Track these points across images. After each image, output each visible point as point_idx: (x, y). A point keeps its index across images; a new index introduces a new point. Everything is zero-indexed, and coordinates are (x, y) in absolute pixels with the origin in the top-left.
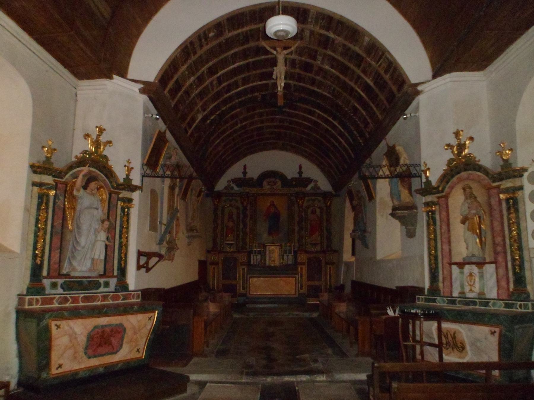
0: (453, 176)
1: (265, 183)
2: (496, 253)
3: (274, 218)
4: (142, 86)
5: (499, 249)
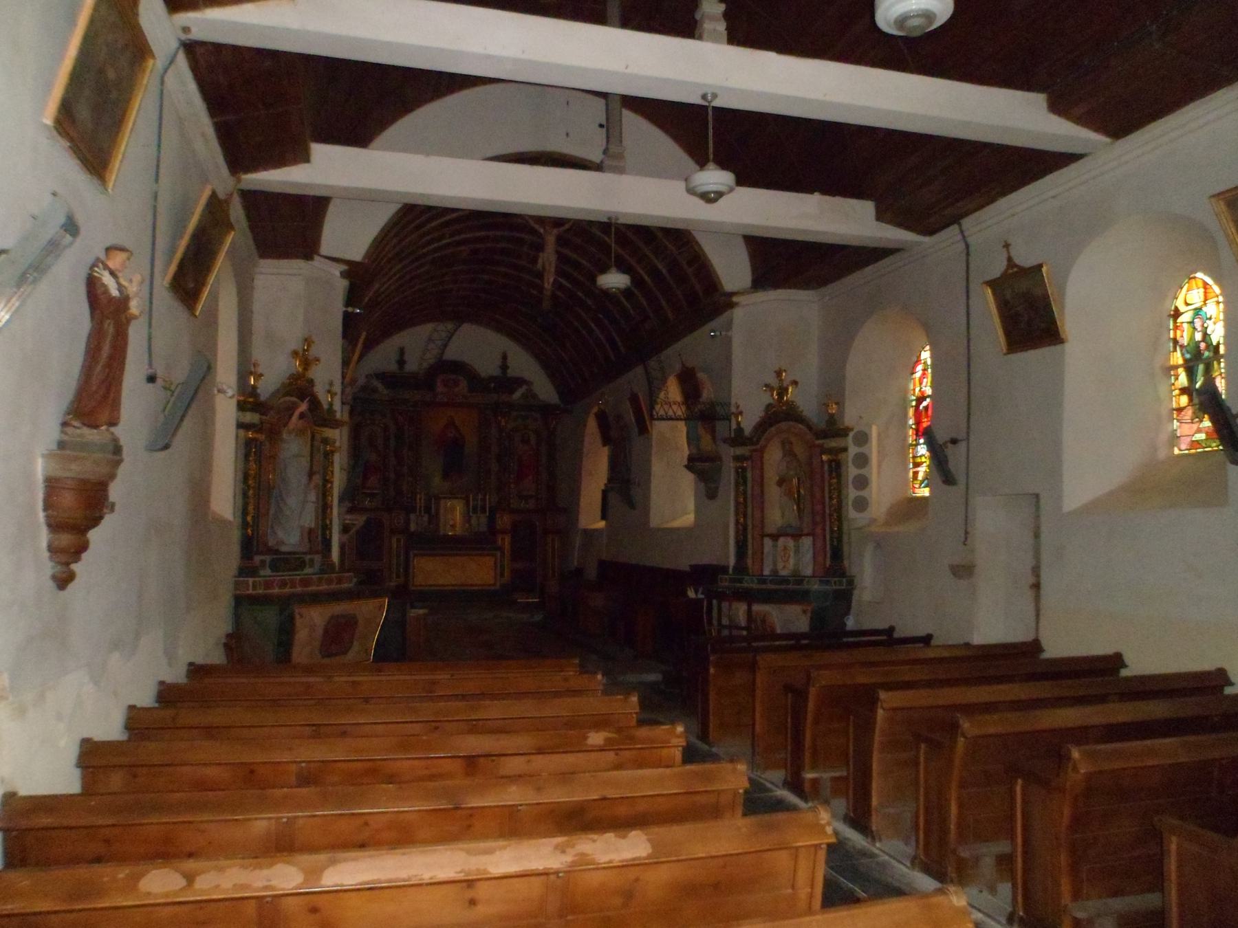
0: (771, 426)
2: (815, 523)
3: (452, 450)
4: (344, 267)
5: (818, 519)
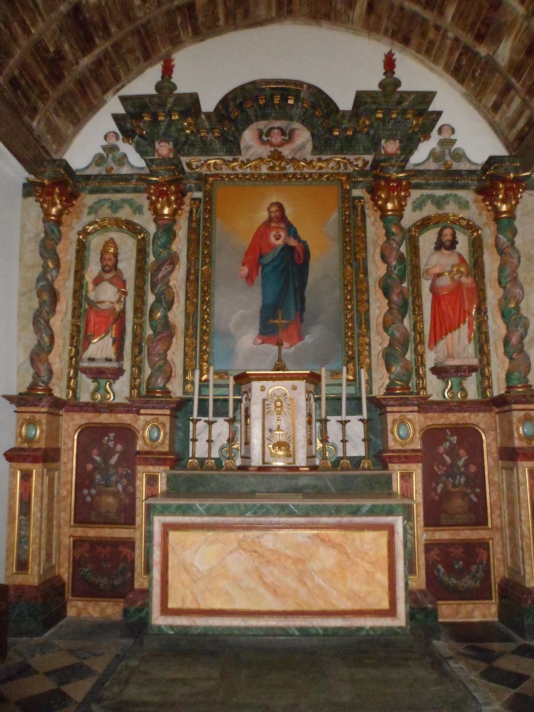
1: (248, 137)
3: (284, 274)
